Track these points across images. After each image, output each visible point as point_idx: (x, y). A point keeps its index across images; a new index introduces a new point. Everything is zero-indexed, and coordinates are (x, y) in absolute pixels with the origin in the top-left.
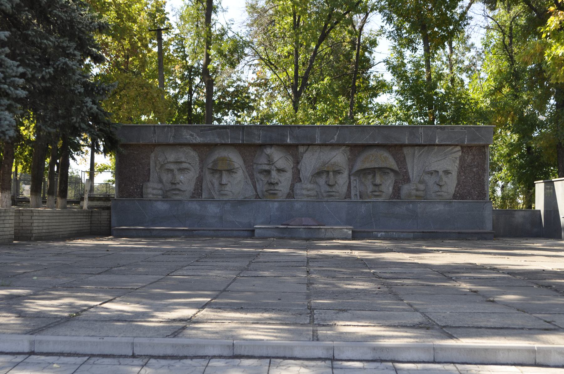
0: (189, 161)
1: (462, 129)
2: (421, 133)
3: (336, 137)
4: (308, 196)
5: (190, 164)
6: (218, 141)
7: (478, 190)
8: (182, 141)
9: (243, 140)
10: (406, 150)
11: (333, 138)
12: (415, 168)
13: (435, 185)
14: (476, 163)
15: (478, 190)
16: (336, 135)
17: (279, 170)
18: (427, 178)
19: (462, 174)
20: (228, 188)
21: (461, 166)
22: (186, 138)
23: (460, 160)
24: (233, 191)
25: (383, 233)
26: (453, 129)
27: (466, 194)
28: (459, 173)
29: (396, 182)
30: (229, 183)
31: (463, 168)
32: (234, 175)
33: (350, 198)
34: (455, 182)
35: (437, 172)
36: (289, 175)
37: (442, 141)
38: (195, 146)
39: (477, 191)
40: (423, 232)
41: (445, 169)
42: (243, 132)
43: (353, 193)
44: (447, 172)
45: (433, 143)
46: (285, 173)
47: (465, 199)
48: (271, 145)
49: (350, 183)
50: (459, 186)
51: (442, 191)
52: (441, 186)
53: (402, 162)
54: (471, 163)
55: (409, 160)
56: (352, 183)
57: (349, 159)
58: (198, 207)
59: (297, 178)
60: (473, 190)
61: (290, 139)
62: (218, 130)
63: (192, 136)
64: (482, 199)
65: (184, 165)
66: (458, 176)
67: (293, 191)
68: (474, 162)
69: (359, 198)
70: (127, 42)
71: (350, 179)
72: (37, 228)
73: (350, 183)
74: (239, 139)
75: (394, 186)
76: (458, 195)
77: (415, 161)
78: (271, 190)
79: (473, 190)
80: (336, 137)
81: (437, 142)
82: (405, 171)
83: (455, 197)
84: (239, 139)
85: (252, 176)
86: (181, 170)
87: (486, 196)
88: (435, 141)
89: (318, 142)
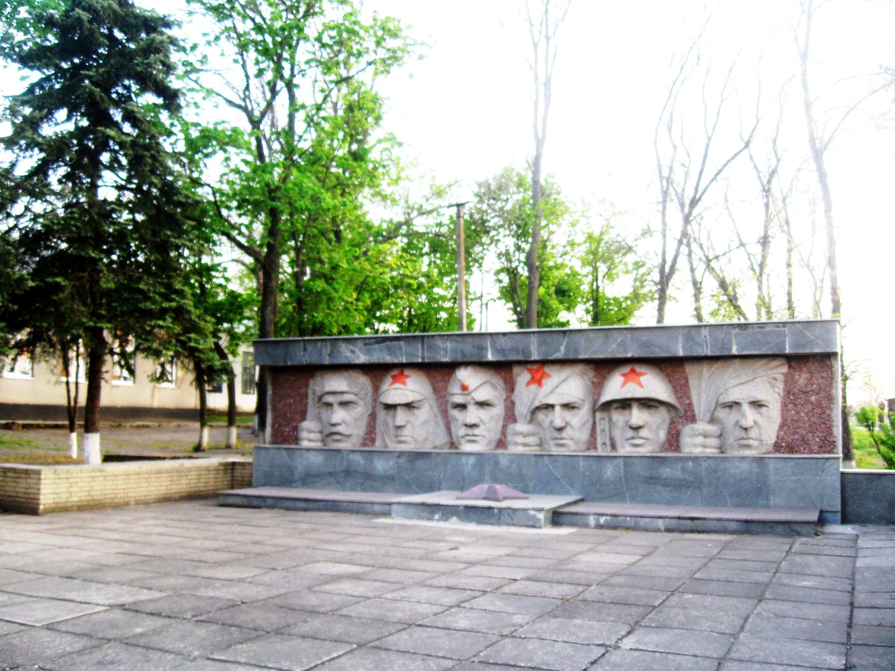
0: (353, 390)
1: (777, 327)
2: (705, 337)
3: (562, 348)
4: (525, 445)
5: (356, 395)
6: (388, 359)
7: (820, 435)
8: (341, 361)
9: (423, 358)
10: (690, 370)
11: (558, 350)
12: (704, 397)
13: (737, 427)
14: (815, 386)
15: (820, 435)
16: (561, 344)
17: (482, 404)
18: (722, 414)
19: (790, 406)
20: (406, 432)
21: (788, 393)
22: (346, 357)
23: (786, 381)
24: (416, 436)
25: (609, 518)
26: (762, 328)
27: (798, 443)
28: (784, 406)
29: (672, 422)
30: (409, 426)
31: (791, 397)
32: (416, 412)
33: (595, 448)
34: (778, 420)
35: (737, 404)
36: (499, 410)
37: (743, 349)
38: (365, 368)
39: (818, 437)
40: (679, 518)
41: (752, 399)
42: (423, 345)
43: (599, 441)
44: (757, 404)
45: (726, 353)
46: (489, 408)
47: (797, 452)
48: (466, 364)
49: (594, 423)
50: (785, 428)
51: (749, 438)
52: (746, 429)
53: (681, 388)
54: (806, 386)
55: (693, 382)
56: (598, 424)
57: (593, 383)
58: (362, 462)
59: (510, 416)
60: (810, 435)
61: (493, 354)
62: (388, 343)
63: (353, 352)
64: (829, 452)
65: (347, 397)
66: (782, 410)
67: (505, 437)
68: (812, 385)
69: (609, 448)
70: (524, 295)
71: (594, 417)
72: (23, 490)
73: (594, 423)
74: (418, 356)
75: (670, 428)
76: (783, 444)
77: (704, 385)
78: (468, 435)
79: (810, 435)
80: (562, 348)
81: (735, 351)
82: (687, 402)
83: (777, 447)
84: (418, 356)
85: (445, 413)
86: (344, 404)
87: (835, 446)
88: (731, 349)
89: (535, 357)
